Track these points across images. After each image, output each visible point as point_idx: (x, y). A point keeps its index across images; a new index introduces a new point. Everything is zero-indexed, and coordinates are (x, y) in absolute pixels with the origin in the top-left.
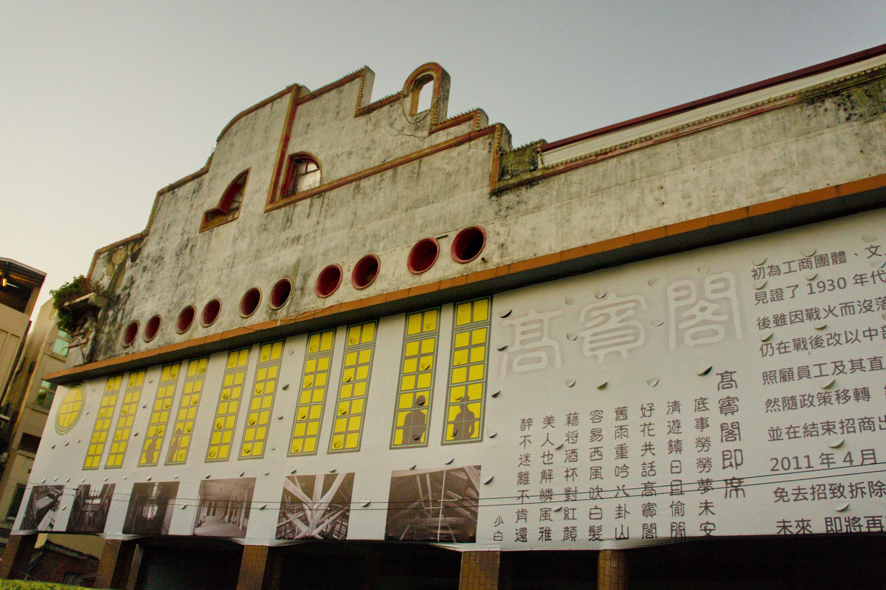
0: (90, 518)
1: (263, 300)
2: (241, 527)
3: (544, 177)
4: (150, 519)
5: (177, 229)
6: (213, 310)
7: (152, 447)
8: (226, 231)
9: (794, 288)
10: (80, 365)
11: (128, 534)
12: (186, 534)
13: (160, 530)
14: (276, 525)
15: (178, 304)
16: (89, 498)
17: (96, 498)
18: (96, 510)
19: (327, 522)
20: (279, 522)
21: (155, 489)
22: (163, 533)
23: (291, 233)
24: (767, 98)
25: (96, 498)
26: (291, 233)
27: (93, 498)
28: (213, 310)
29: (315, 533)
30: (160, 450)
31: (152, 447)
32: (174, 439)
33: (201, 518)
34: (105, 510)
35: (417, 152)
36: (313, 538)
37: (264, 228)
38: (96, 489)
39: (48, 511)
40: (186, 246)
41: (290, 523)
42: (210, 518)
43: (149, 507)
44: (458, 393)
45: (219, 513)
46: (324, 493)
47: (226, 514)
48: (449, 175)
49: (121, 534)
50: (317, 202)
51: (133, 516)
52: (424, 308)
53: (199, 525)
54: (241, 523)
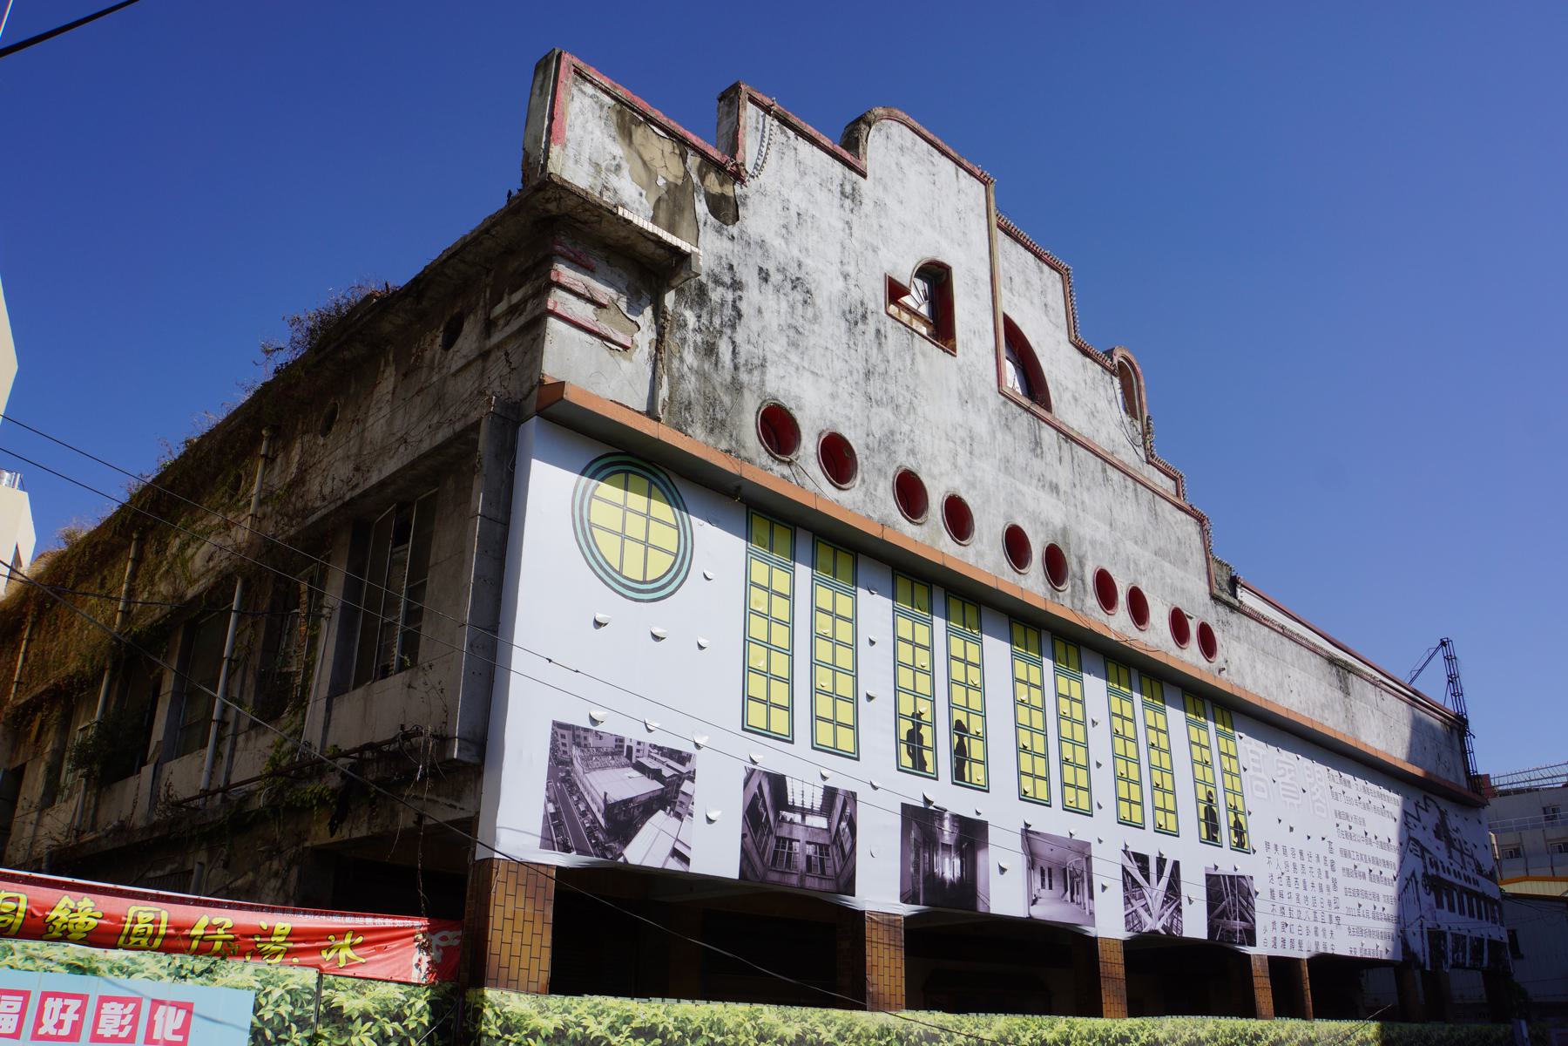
0: (809, 858)
1: (1034, 553)
2: (1088, 913)
4: (952, 883)
7: (914, 738)
9: (1416, 815)
10: (639, 412)
11: (913, 903)
12: (1022, 916)
13: (974, 907)
14: (1123, 913)
18: (820, 841)
19: (1167, 914)
20: (1126, 909)
22: (981, 908)
24: (1297, 632)
25: (812, 812)
29: (1159, 927)
30: (934, 749)
31: (914, 738)
32: (956, 739)
33: (1035, 891)
34: (847, 847)
35: (1087, 439)
36: (1156, 932)
38: (804, 791)
39: (653, 812)
41: (1135, 911)
42: (1045, 893)
43: (943, 859)
44: (907, 707)
45: (1058, 887)
46: (1159, 879)
47: (1066, 890)
49: (898, 902)
51: (917, 870)
52: (917, 578)
53: (1034, 902)
54: (1087, 906)
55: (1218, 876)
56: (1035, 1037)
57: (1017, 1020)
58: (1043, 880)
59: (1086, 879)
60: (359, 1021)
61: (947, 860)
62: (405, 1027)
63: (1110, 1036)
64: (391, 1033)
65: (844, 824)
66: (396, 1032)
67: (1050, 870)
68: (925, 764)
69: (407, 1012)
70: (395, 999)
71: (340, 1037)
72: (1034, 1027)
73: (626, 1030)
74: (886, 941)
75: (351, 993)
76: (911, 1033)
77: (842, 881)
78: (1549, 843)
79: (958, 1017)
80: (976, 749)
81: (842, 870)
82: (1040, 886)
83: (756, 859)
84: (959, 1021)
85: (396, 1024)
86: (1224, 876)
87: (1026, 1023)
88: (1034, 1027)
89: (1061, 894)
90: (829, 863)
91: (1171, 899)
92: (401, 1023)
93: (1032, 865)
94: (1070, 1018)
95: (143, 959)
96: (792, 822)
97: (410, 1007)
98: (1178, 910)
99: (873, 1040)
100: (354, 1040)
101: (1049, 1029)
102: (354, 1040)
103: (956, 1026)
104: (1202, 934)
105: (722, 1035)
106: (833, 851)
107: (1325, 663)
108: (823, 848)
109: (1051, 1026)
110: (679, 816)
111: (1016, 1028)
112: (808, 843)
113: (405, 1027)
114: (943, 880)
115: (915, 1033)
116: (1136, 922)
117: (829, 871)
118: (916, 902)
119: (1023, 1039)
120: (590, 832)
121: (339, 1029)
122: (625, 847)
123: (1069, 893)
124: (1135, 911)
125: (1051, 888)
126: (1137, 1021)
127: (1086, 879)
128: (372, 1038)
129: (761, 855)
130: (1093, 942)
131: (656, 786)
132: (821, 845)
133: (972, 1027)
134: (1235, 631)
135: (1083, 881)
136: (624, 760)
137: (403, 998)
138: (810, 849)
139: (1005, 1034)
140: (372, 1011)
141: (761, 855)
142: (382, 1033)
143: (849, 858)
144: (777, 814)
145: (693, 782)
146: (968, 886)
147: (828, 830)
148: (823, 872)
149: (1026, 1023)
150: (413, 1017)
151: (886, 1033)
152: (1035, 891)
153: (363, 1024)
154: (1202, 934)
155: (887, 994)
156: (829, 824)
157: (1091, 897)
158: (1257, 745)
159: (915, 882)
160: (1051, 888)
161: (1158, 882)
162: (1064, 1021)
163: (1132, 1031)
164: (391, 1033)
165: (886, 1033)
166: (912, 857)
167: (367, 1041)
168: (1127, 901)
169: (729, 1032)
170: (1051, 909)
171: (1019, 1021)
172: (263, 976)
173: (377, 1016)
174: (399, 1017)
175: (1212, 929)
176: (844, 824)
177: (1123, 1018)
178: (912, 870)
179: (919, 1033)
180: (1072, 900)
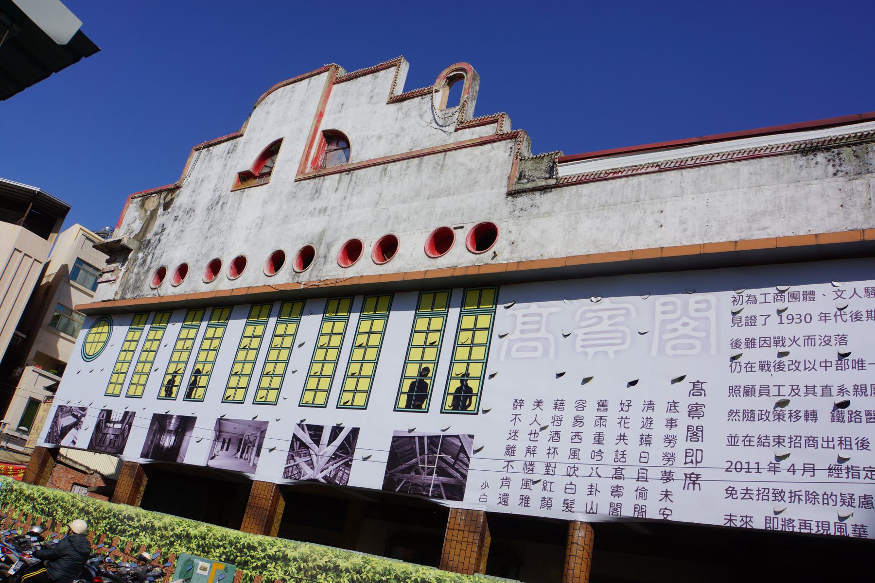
0: (111, 440)
2: (251, 464)
3: (557, 186)
5: (209, 186)
6: (240, 264)
7: (171, 382)
8: (256, 194)
15: (206, 255)
16: (111, 422)
17: (117, 422)
18: (117, 433)
19: (331, 468)
20: (287, 463)
21: (173, 421)
23: (318, 204)
25: (117, 422)
26: (318, 204)
27: (115, 423)
28: (240, 264)
30: (179, 386)
31: (171, 382)
32: (193, 378)
33: (215, 452)
37: (293, 196)
40: (217, 202)
43: (166, 437)
44: (460, 369)
45: (232, 449)
47: (238, 451)
48: (470, 171)
50: (345, 177)
51: (152, 443)
53: (213, 458)
55: (414, 437)
56: (149, 522)
57: (177, 519)
58: (223, 446)
59: (256, 445)
60: (292, 561)
61: (168, 437)
62: (361, 577)
63: (239, 543)
64: (355, 579)
65: (127, 426)
66: (304, 566)
67: (230, 440)
68: (172, 393)
69: (363, 570)
70: (360, 564)
71: (337, 579)
72: (185, 525)
73: (42, 497)
74: (128, 474)
75: (344, 560)
76: (121, 514)
77: (119, 449)
78: (790, 300)
79: (147, 512)
80: (203, 381)
81: (121, 443)
82: (219, 449)
83: (94, 442)
84: (147, 514)
85: (358, 575)
86: (421, 438)
87: (181, 522)
88: (185, 525)
89: (234, 453)
90: (117, 442)
91: (340, 457)
92: (360, 575)
93: (217, 438)
94: (210, 525)
95: (463, 578)
96: (109, 427)
97: (364, 568)
98: (348, 465)
99: (217, 541)
100: (342, 580)
101: (158, 521)
102: (342, 580)
103: (271, 544)
104: (377, 483)
105: (63, 502)
106: (120, 437)
107: (801, 160)
108: (117, 436)
109: (196, 527)
110: (77, 429)
111: (141, 515)
112: (112, 434)
113: (361, 577)
114: (163, 447)
115: (242, 543)
116: (295, 472)
117: (116, 445)
118: (147, 457)
119: (176, 530)
120: (56, 436)
121: (337, 575)
122: (62, 440)
123: (239, 453)
124: (297, 465)
125: (227, 450)
126: (143, 511)
127: (256, 445)
128: (348, 580)
129: (96, 440)
130: (250, 482)
131: (75, 420)
132: (116, 435)
133: (282, 546)
134: (544, 209)
135: (254, 446)
136: (70, 413)
137: (309, 553)
138: (112, 437)
139: (167, 525)
140: (350, 568)
141: (96, 440)
142: (299, 566)
143: (125, 439)
144: (105, 424)
145: (294, 434)
146: (176, 449)
147: (121, 429)
148: (114, 445)
149: (181, 522)
150: (365, 573)
151: (224, 539)
152: (215, 452)
153: (346, 573)
154: (377, 483)
155: (120, 496)
156: (122, 426)
157: (258, 455)
158: (539, 307)
159: (149, 448)
160: (227, 450)
161: (329, 444)
162: (360, 557)
163: (137, 515)
164: (355, 579)
165: (224, 539)
166: (152, 437)
167: (346, 581)
168: (291, 457)
169: (65, 502)
170: (225, 461)
171: (177, 520)
172: (365, 560)
173: (351, 571)
174: (359, 572)
175: (389, 481)
176: (127, 426)
177: (256, 534)
178: (149, 443)
179: (244, 544)
180: (241, 457)
